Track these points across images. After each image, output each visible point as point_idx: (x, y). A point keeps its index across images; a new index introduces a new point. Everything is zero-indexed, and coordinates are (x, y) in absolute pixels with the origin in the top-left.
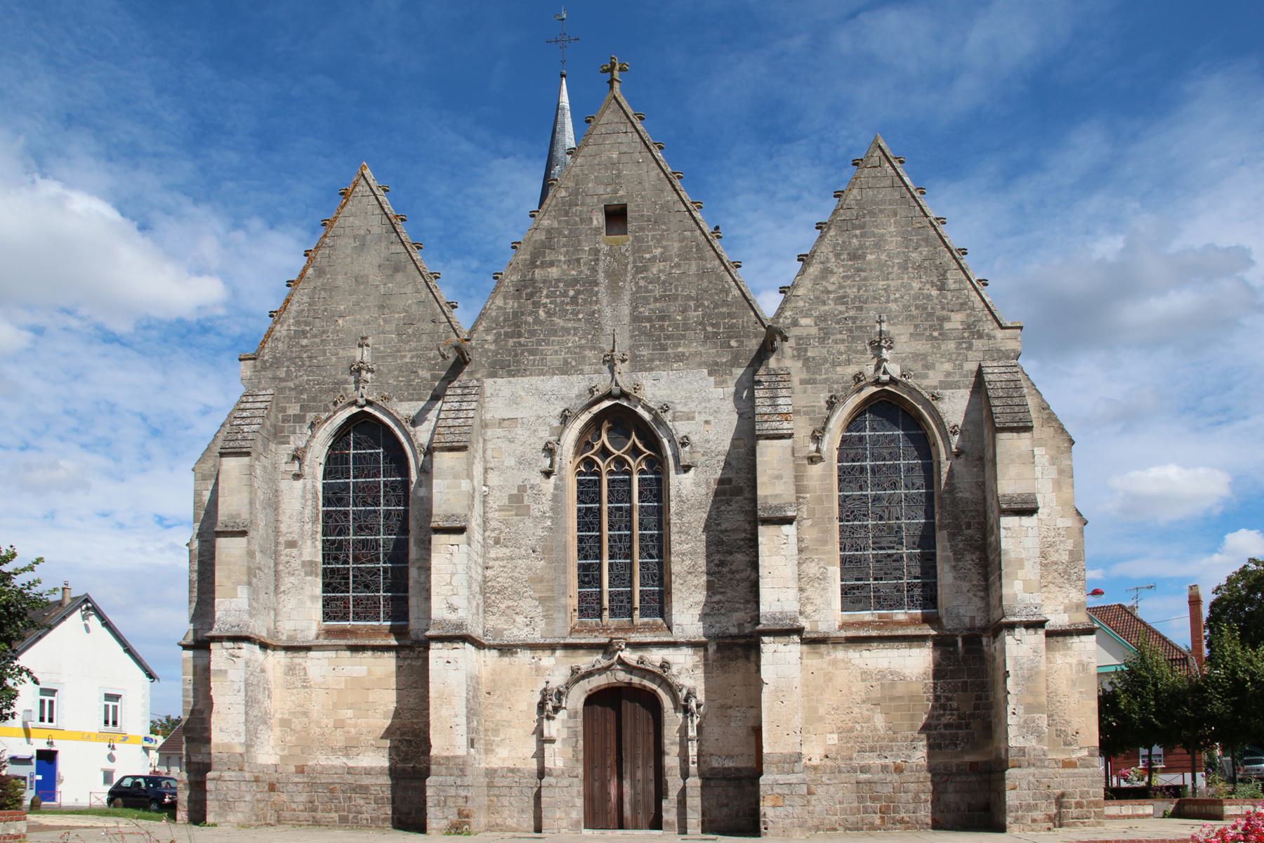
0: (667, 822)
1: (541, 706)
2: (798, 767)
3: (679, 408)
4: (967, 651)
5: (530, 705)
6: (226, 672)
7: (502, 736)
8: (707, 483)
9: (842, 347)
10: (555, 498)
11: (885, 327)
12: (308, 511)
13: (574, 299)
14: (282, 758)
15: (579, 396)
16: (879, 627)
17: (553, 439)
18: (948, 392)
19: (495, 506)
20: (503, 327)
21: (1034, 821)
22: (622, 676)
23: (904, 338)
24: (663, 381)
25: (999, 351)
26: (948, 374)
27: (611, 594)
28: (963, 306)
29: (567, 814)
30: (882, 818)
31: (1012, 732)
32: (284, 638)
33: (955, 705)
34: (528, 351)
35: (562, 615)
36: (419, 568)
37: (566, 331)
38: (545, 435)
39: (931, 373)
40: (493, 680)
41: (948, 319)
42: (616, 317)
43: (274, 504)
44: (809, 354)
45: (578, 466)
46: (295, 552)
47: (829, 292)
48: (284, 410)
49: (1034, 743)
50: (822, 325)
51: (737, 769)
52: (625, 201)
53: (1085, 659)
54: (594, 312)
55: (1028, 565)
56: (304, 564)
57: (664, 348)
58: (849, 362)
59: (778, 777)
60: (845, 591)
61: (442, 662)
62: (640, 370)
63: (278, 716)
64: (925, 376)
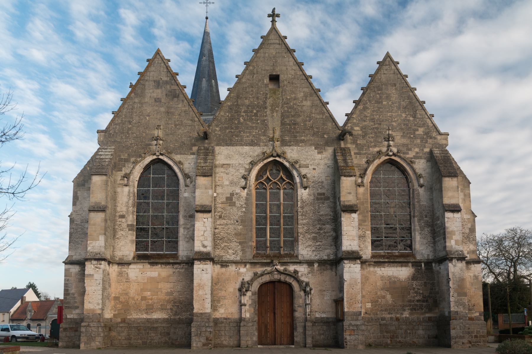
0: (296, 342)
1: (240, 290)
2: (360, 318)
3: (302, 162)
4: (426, 269)
5: (235, 289)
6: (93, 275)
7: (221, 303)
8: (314, 194)
9: (372, 140)
10: (247, 199)
11: (390, 132)
12: (131, 202)
13: (256, 115)
14: (114, 315)
15: (258, 156)
16: (387, 258)
17: (246, 173)
18: (417, 160)
19: (220, 202)
20: (224, 124)
21: (463, 343)
22: (276, 277)
23: (398, 137)
24: (295, 151)
25: (439, 144)
26: (417, 153)
27: (270, 241)
28: (423, 125)
29: (251, 338)
30: (391, 340)
31: (452, 304)
32: (117, 259)
33: (421, 292)
34: (235, 135)
35: (250, 250)
36: (184, 228)
37: (252, 128)
38: (243, 172)
39: (410, 152)
40: (218, 278)
41: (418, 130)
42: (274, 122)
43: (114, 198)
44: (358, 142)
45: (256, 186)
46: (124, 220)
47: (367, 117)
48: (120, 156)
49: (462, 309)
50: (364, 130)
51: (327, 318)
52: (278, 73)
53: (476, 274)
54: (265, 120)
55: (457, 233)
56: (128, 225)
57: (295, 137)
58: (375, 146)
59: (351, 322)
60: (373, 242)
61: (199, 270)
62: (285, 146)
63: (113, 295)
64: (408, 154)
